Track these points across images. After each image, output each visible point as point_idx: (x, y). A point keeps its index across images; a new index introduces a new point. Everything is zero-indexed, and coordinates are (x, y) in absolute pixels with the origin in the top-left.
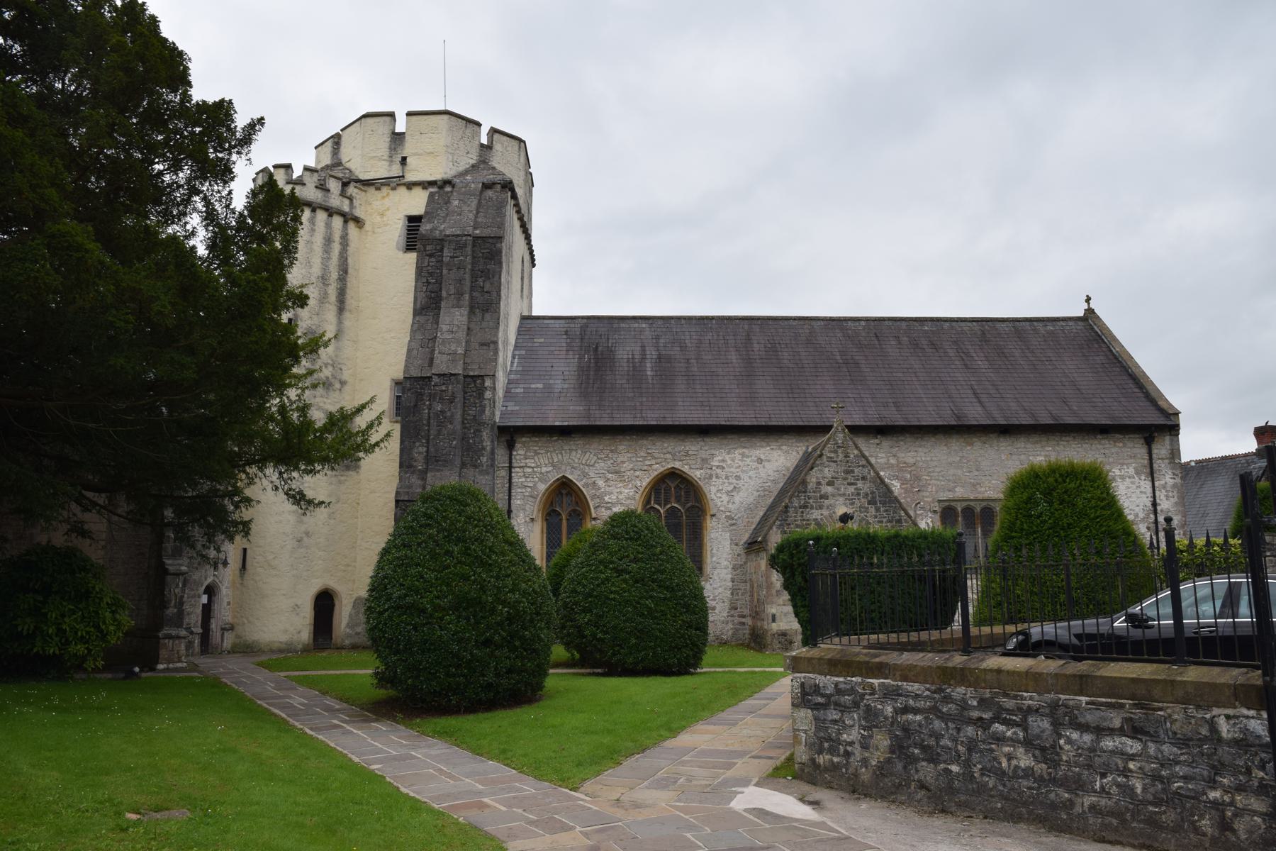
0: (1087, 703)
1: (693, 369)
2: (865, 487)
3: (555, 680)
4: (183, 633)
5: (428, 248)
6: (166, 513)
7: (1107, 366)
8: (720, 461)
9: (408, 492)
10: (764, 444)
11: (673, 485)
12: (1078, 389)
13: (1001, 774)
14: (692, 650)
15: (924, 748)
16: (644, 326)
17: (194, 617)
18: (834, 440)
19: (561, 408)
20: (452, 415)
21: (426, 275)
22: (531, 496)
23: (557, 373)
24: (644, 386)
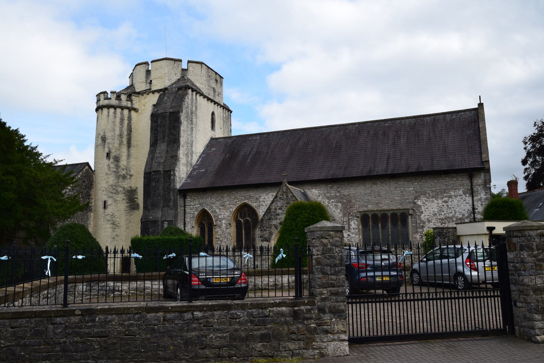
8: (263, 199)
18: (282, 190)
22: (193, 217)
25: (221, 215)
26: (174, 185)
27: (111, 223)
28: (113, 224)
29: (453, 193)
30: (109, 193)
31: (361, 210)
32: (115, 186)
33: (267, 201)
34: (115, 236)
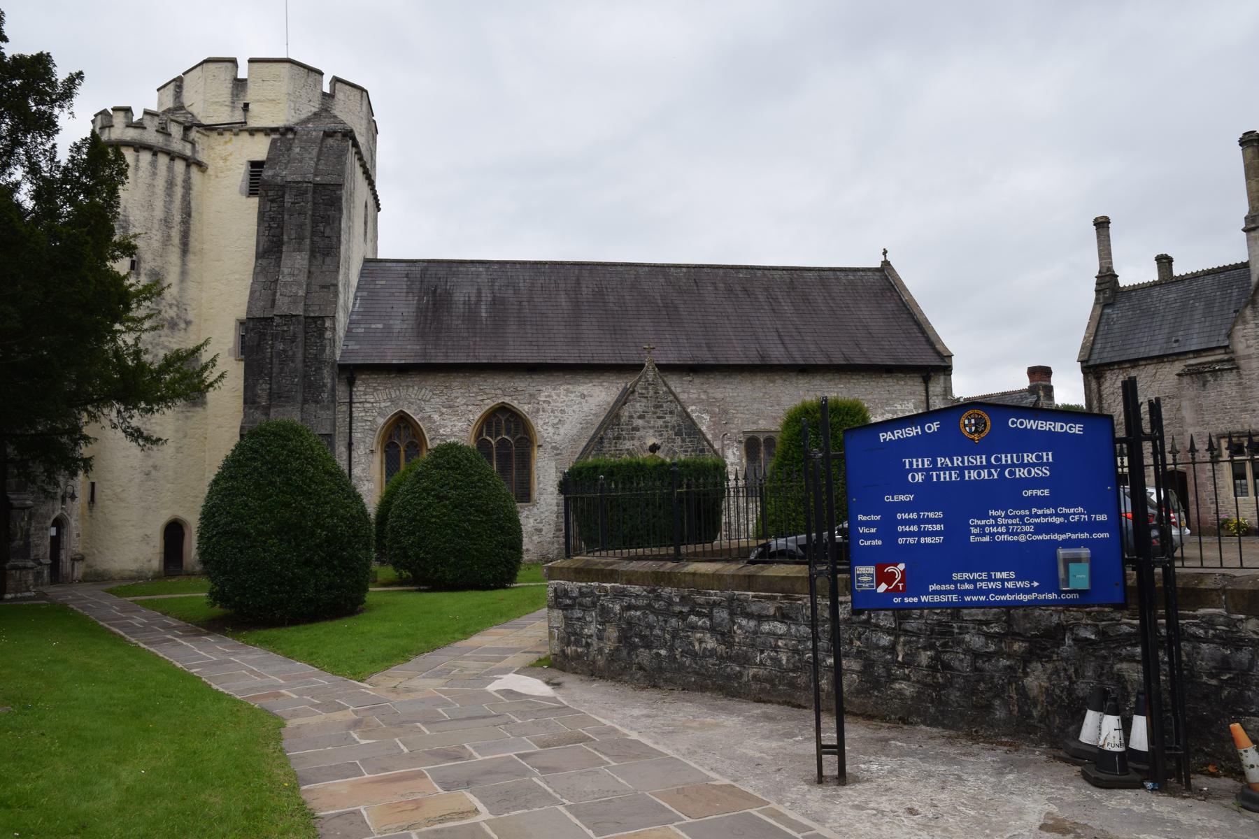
0: (753, 597)
1: (525, 311)
2: (672, 420)
3: (374, 594)
4: (30, 564)
5: (270, 193)
6: (8, 450)
7: (897, 313)
8: (546, 397)
10: (587, 381)
11: (503, 419)
12: (870, 333)
13: (694, 655)
14: (506, 567)
15: (643, 638)
16: (481, 269)
17: (43, 549)
18: (646, 378)
19: (399, 347)
20: (294, 354)
21: (268, 219)
23: (396, 314)
24: (478, 326)
29: (899, 407)
31: (748, 428)
32: (151, 343)
33: (555, 401)
34: (151, 469)
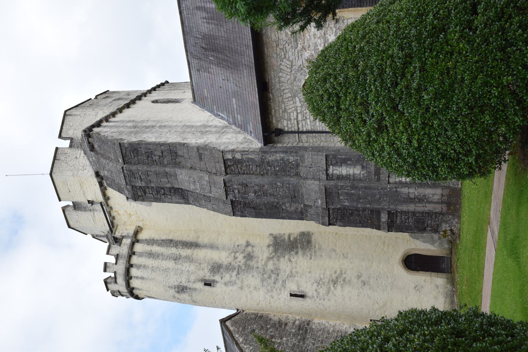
9: (322, 217)
16: (184, 5)
20: (257, 185)
21: (159, 196)
25: (316, 45)
26: (253, 152)
27: (334, 286)
28: (335, 282)
30: (276, 286)
32: (263, 274)
34: (360, 280)
